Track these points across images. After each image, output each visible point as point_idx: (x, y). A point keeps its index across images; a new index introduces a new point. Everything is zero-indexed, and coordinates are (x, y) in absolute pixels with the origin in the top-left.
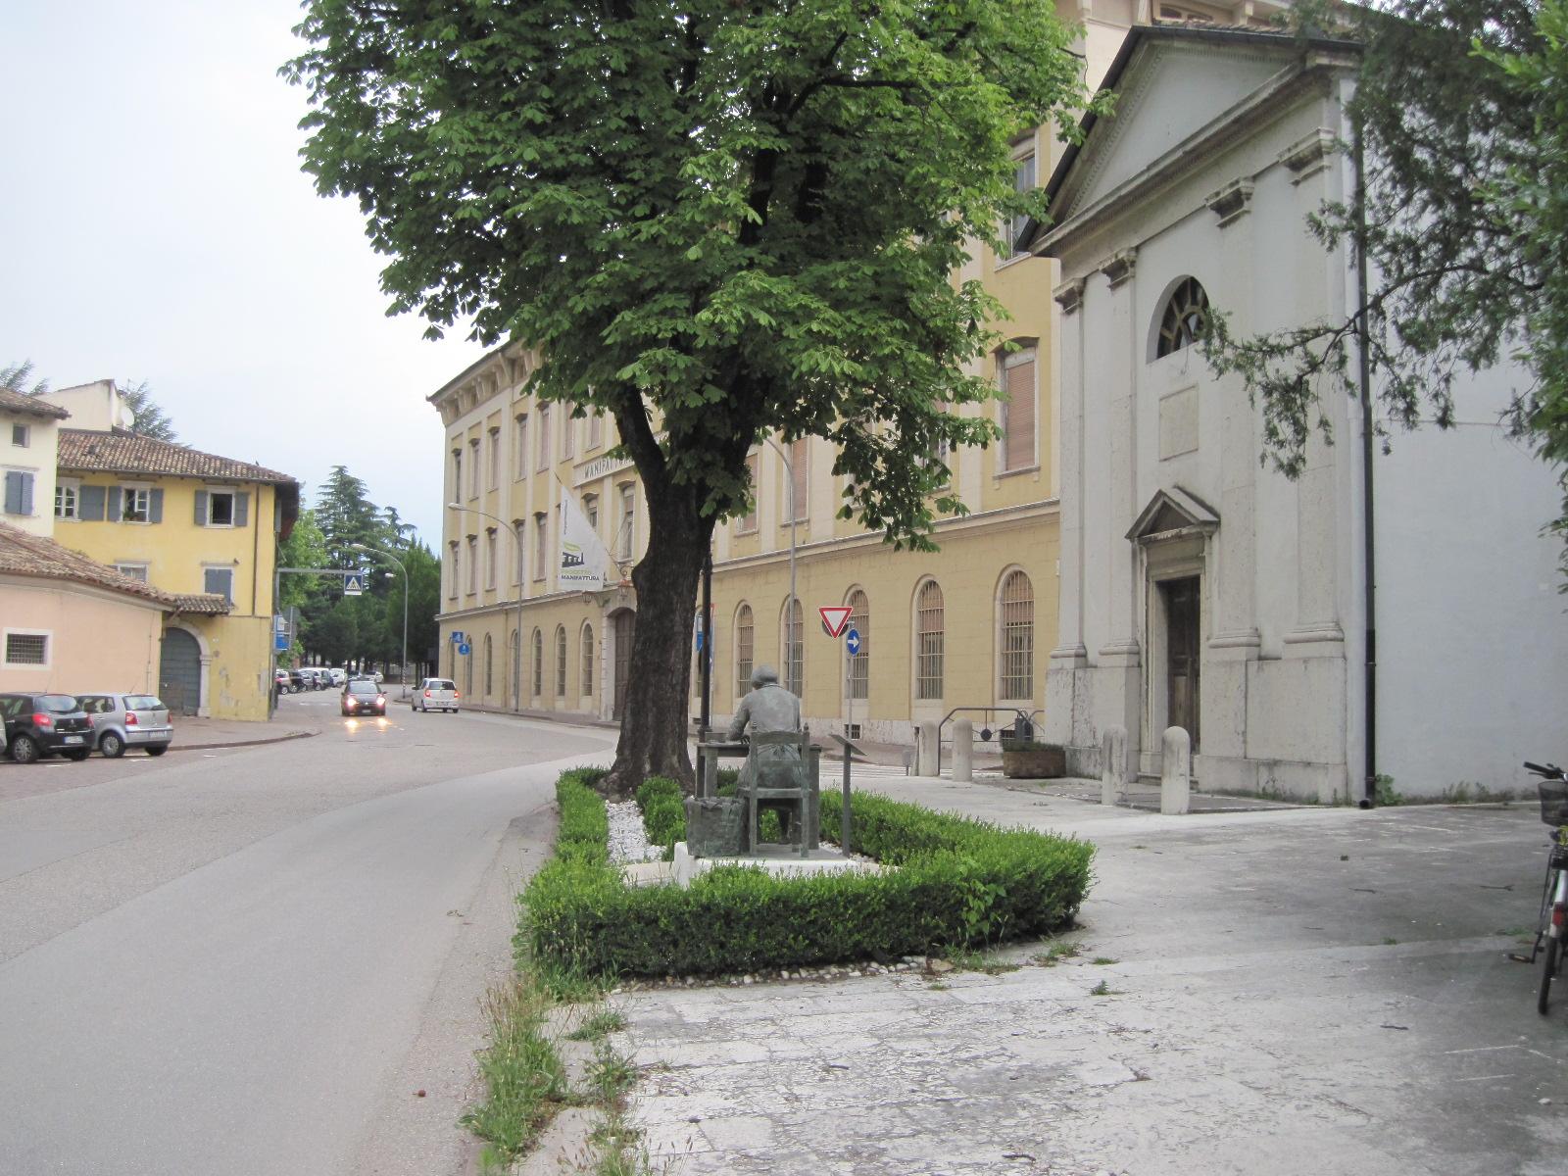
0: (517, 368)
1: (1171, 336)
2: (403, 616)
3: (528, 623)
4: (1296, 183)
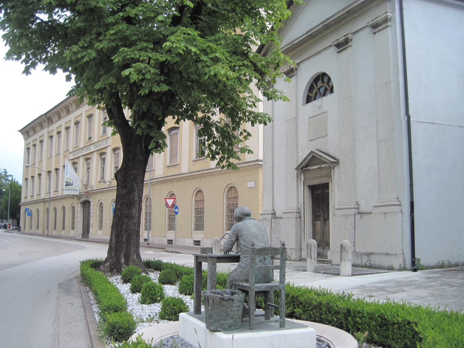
0: (50, 121)
1: (312, 95)
2: (8, 203)
3: (52, 205)
4: (375, 33)
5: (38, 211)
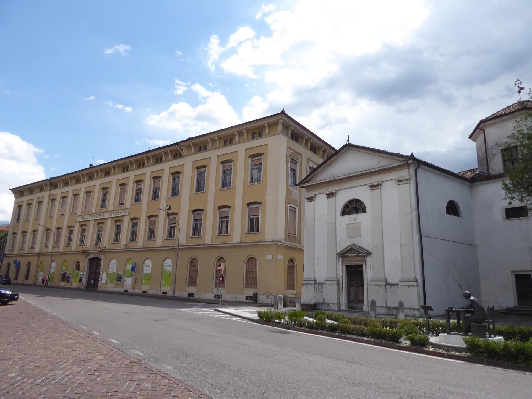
5: (29, 264)
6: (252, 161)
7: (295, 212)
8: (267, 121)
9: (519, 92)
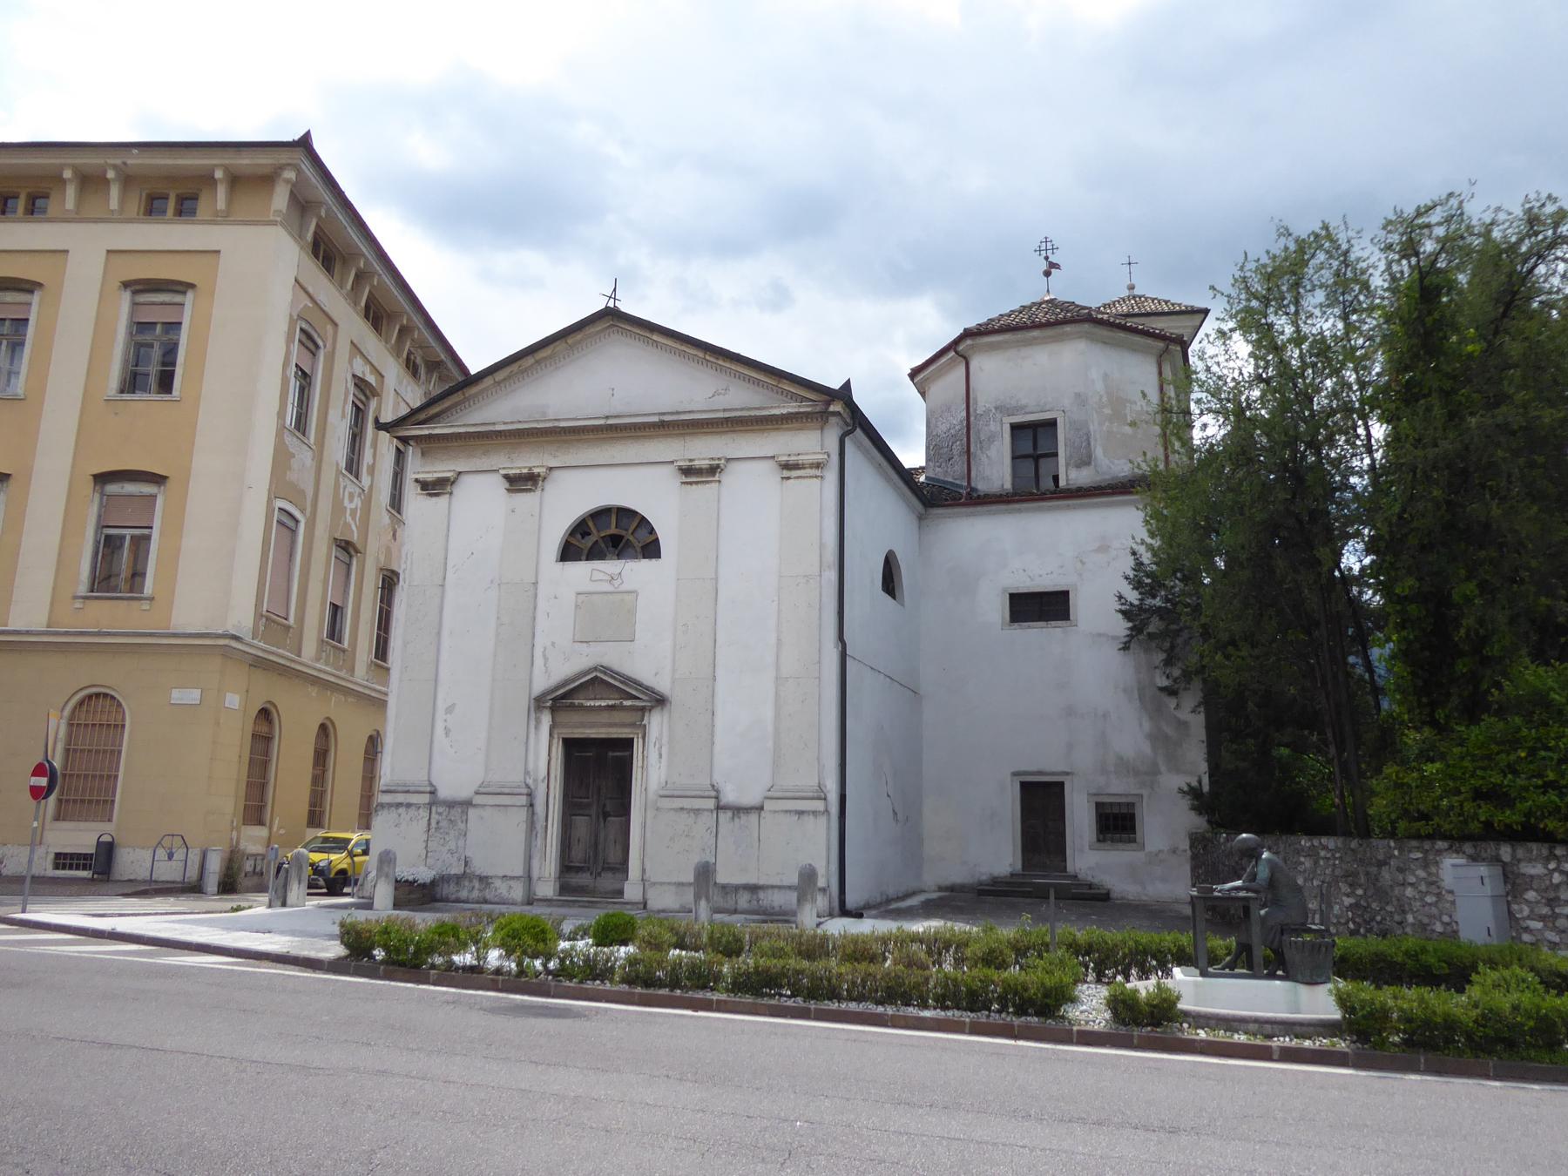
6: (135, 304)
7: (294, 532)
8: (227, 162)
9: (1047, 274)
